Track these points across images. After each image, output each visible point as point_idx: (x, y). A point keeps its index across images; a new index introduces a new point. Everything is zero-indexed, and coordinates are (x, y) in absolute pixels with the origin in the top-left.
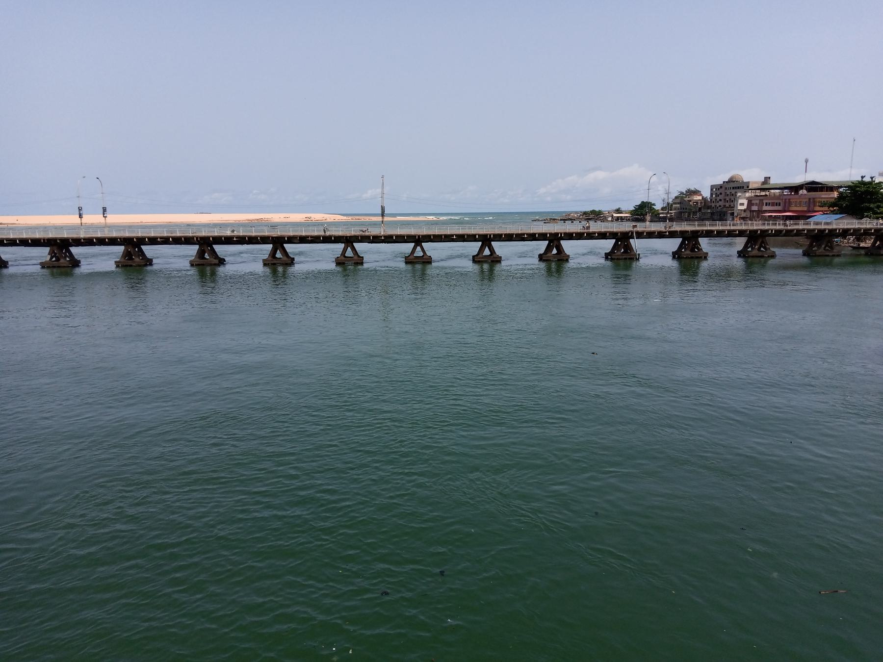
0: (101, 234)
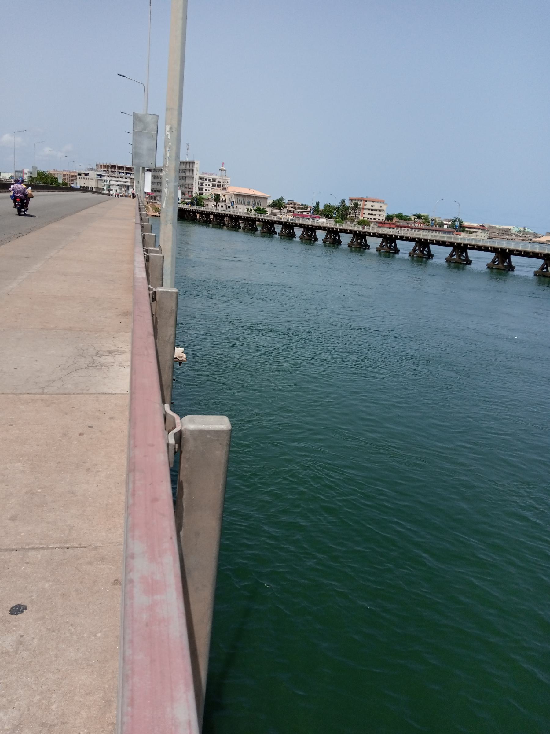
0: (497, 245)
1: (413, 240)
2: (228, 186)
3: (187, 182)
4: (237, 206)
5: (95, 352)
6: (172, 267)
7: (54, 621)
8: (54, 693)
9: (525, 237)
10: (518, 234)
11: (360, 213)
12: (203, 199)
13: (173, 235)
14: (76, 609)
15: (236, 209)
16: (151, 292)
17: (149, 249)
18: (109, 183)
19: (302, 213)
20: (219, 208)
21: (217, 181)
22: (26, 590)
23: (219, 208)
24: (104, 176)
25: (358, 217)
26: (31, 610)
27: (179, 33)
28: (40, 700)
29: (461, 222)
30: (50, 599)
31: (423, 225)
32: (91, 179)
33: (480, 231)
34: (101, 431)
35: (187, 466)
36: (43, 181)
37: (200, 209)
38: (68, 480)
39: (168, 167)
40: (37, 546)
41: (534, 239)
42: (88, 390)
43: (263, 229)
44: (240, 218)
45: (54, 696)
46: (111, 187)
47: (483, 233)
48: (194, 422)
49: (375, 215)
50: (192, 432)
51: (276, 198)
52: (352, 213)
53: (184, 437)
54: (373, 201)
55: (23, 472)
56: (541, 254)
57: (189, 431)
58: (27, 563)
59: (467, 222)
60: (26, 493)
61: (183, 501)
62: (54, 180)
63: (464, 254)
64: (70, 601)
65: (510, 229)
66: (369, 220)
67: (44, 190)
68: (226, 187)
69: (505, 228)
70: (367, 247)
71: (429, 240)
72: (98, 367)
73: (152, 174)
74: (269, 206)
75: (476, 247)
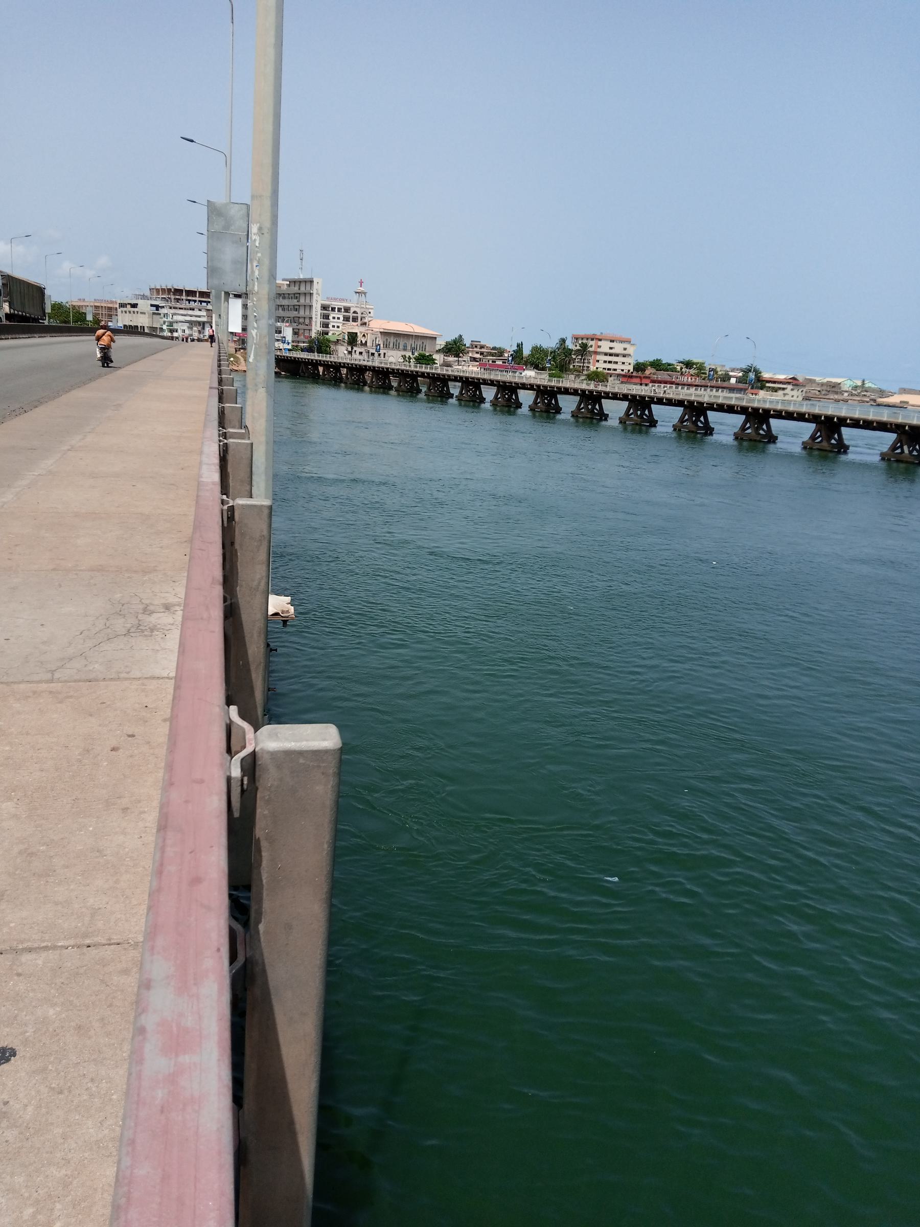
0: (819, 410)
1: (680, 403)
2: (370, 319)
3: (302, 313)
4: (385, 351)
5: (141, 607)
6: (267, 460)
7: (62, 1074)
8: (59, 1202)
9: (865, 395)
10: (854, 392)
11: (591, 361)
12: (329, 341)
13: (267, 407)
14: (99, 1051)
15: (384, 357)
16: (226, 507)
17: (229, 432)
18: (172, 319)
19: (495, 362)
20: (356, 356)
21: (352, 311)
22: (16, 1022)
23: (356, 356)
24: (163, 307)
25: (588, 367)
26: (24, 1056)
27: (270, 70)
28: (34, 1215)
29: (757, 372)
30: (58, 1035)
31: (696, 379)
32: (141, 313)
33: (790, 387)
34: (148, 743)
35: (266, 812)
36: (61, 318)
37: (324, 359)
38: (91, 829)
39: (257, 293)
40: (36, 945)
41: (880, 400)
42: (128, 673)
43: (429, 389)
44: (391, 373)
45: (58, 1206)
46: (175, 326)
47: (795, 391)
48: (277, 735)
49: (616, 363)
50: (274, 754)
51: (451, 337)
52: (577, 360)
53: (260, 763)
54: (613, 339)
55: (15, 817)
56: (891, 424)
57: (269, 752)
58: (19, 975)
59: (767, 372)
60: (20, 853)
61: (262, 871)
62: (80, 316)
63: (764, 427)
64: (90, 1038)
65: (840, 384)
66: (607, 371)
67: (62, 335)
68: (366, 320)
69: (831, 382)
70: (603, 416)
71: (707, 404)
72: (146, 633)
73: (243, 301)
74: (438, 351)
75: (783, 414)
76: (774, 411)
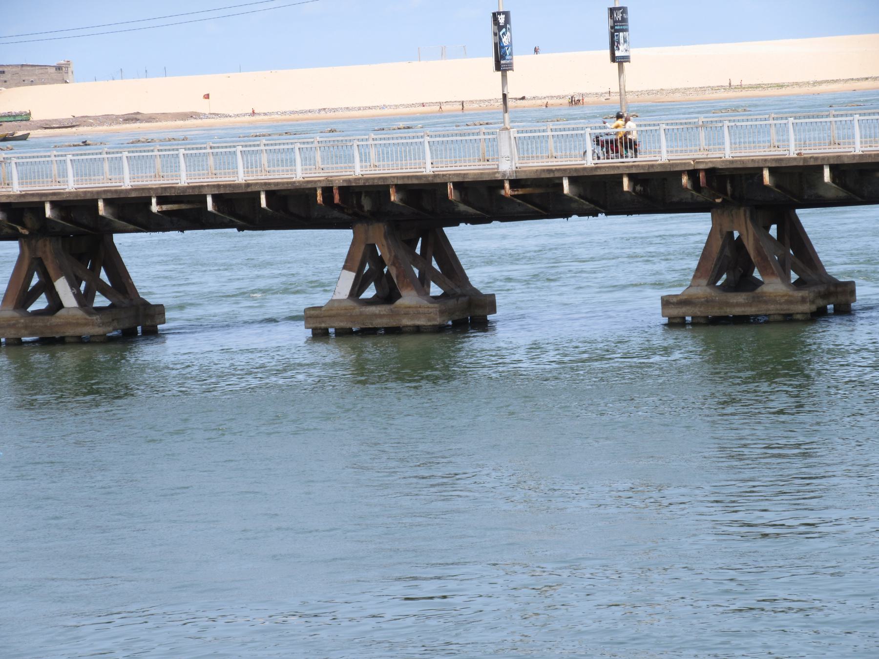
76: (161, 200)
